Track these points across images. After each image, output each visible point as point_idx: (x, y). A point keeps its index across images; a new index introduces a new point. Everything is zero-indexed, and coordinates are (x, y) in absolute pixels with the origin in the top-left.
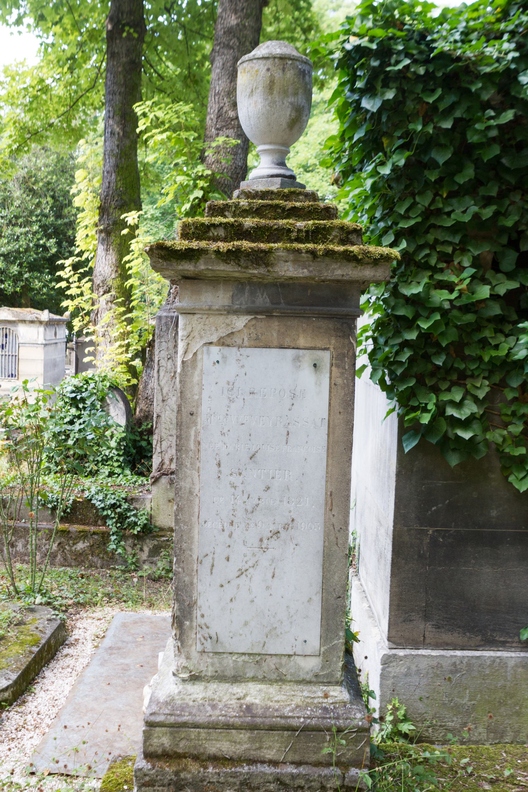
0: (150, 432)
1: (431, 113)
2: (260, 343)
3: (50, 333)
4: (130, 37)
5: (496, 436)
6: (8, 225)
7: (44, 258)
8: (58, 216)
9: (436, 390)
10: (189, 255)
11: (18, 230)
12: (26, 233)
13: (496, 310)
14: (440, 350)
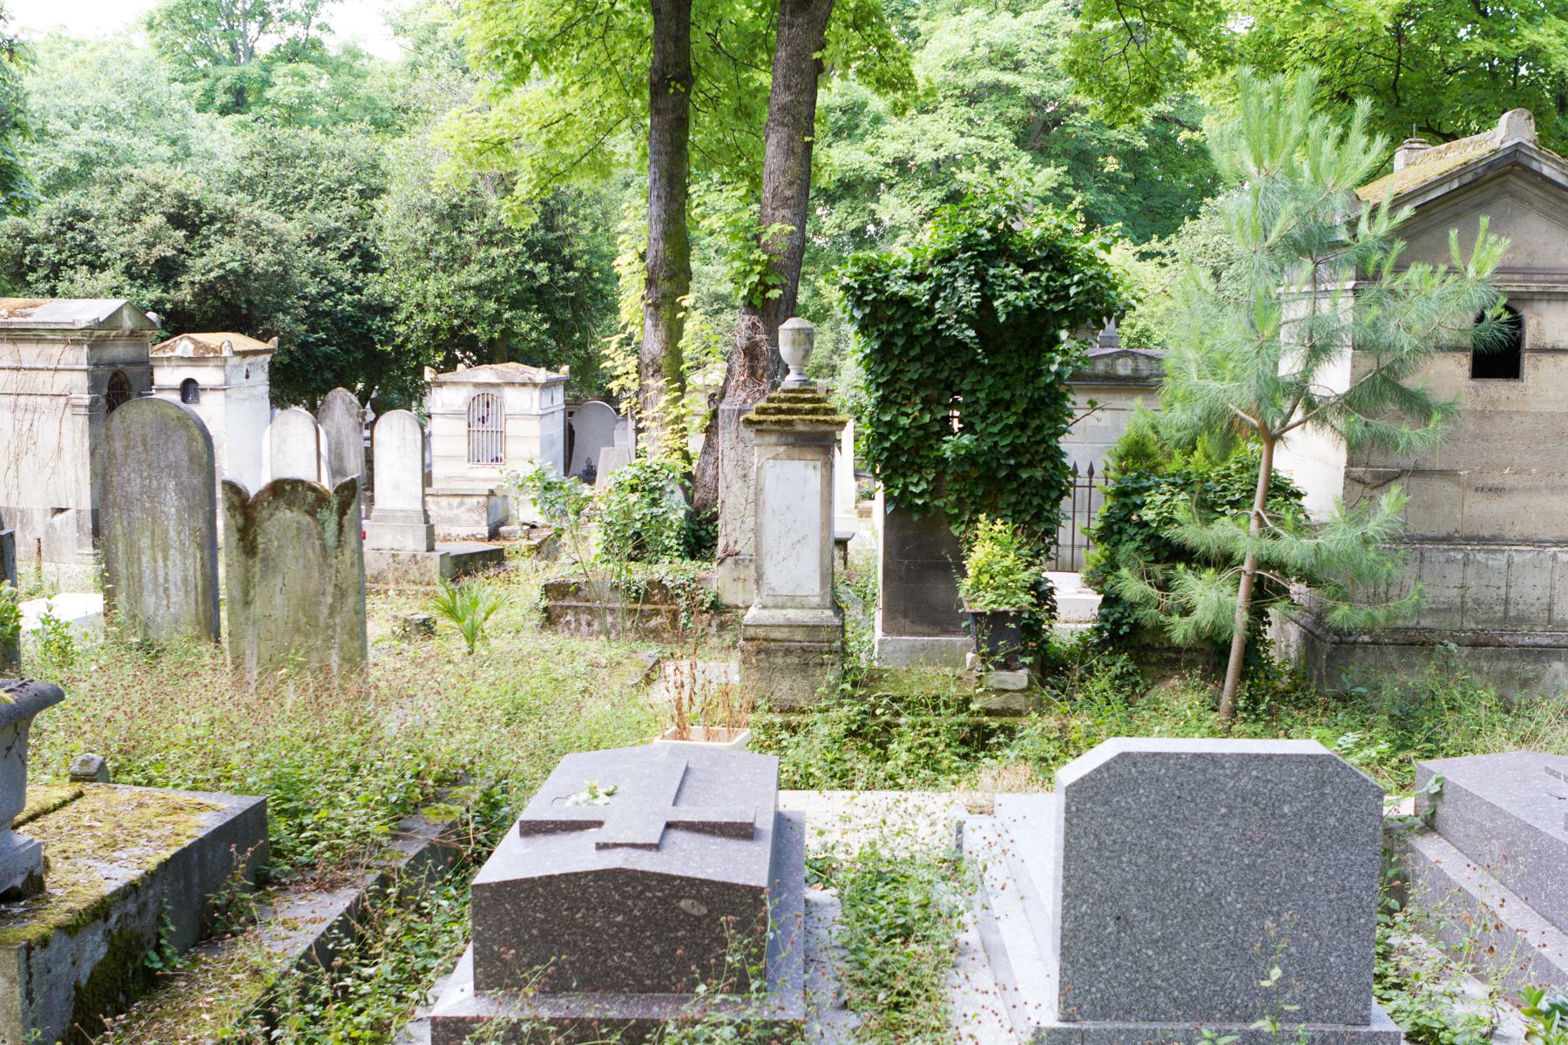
0: (715, 517)
1: (890, 320)
2: (790, 458)
3: (547, 396)
4: (677, 92)
5: (939, 503)
6: (478, 244)
7: (531, 289)
8: (550, 228)
9: (905, 476)
10: (759, 422)
11: (495, 252)
12: (506, 257)
13: (937, 428)
14: (904, 452)
